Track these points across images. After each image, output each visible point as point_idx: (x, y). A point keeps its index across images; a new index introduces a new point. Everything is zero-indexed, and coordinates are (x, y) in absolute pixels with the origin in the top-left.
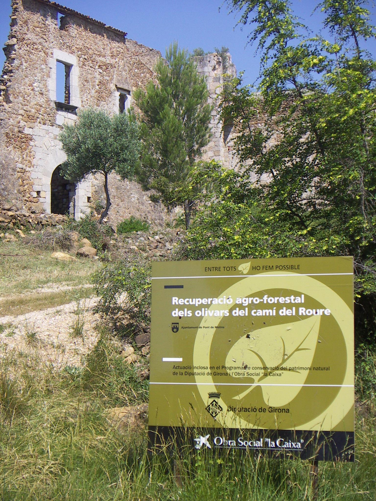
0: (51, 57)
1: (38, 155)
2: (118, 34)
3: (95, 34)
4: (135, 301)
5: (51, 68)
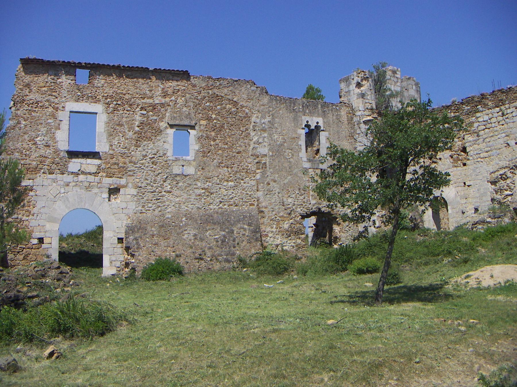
0: (63, 110)
1: (39, 204)
2: (179, 74)
3: (135, 79)
4: (192, 362)
5: (61, 121)
